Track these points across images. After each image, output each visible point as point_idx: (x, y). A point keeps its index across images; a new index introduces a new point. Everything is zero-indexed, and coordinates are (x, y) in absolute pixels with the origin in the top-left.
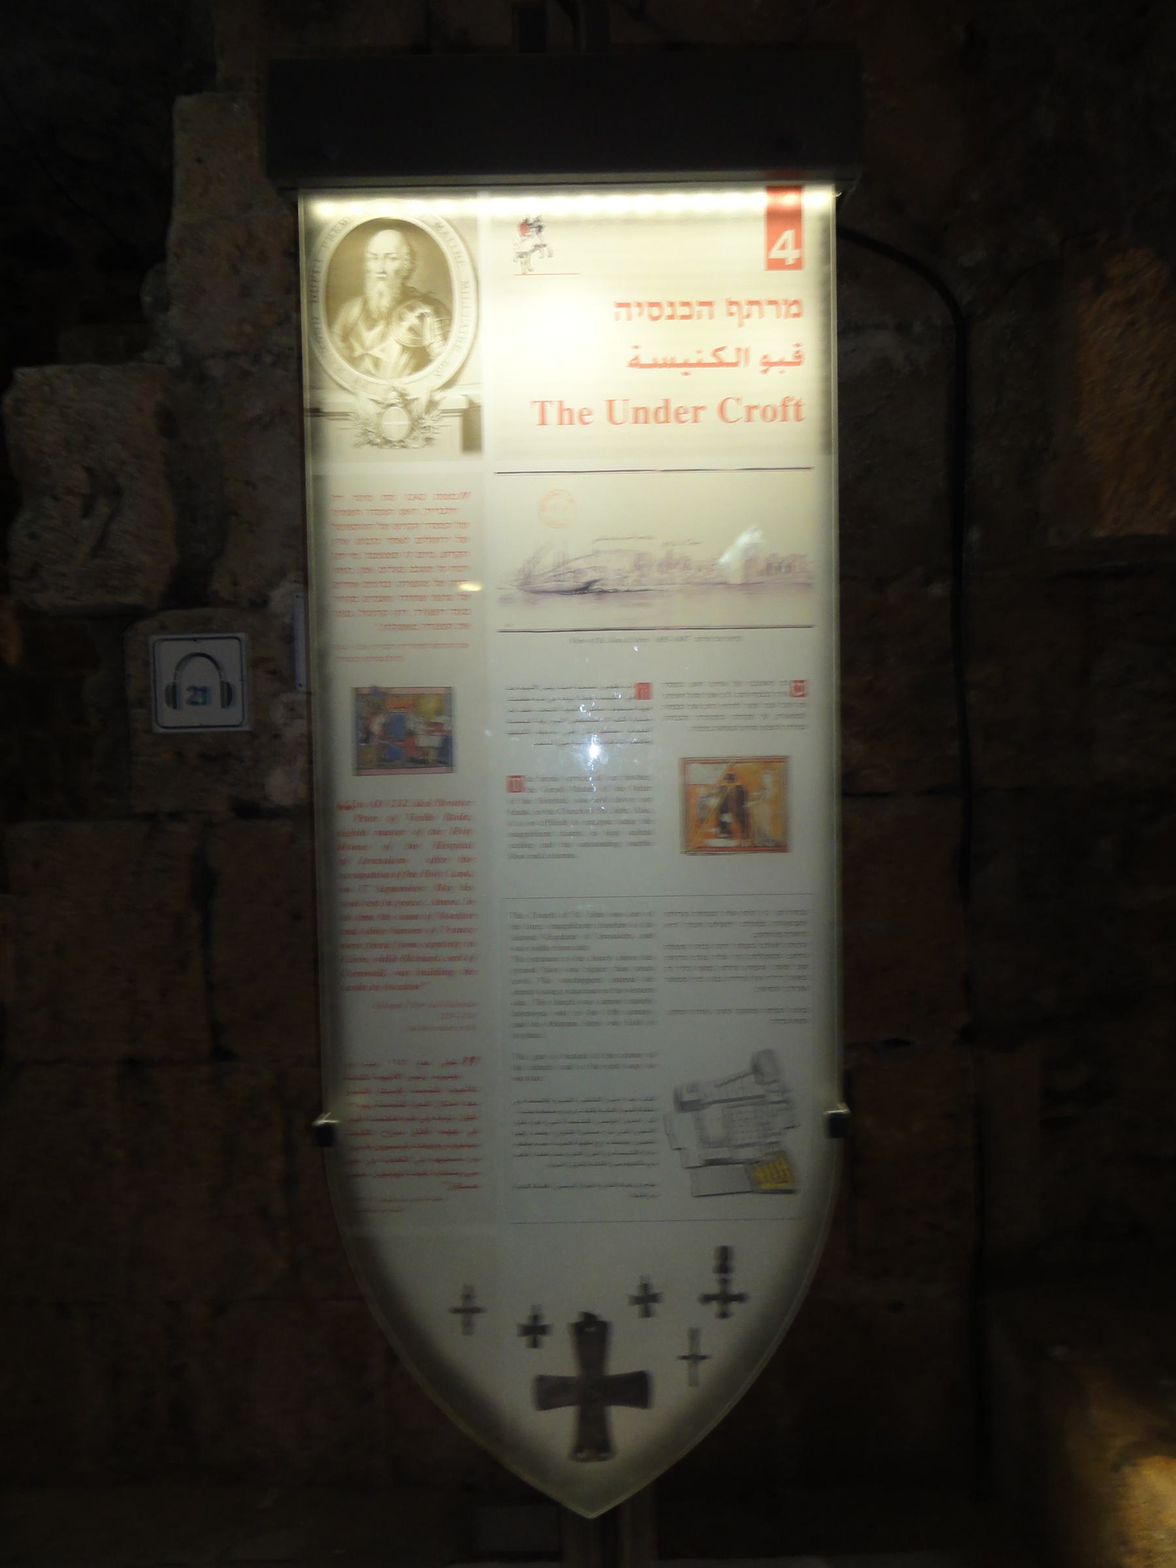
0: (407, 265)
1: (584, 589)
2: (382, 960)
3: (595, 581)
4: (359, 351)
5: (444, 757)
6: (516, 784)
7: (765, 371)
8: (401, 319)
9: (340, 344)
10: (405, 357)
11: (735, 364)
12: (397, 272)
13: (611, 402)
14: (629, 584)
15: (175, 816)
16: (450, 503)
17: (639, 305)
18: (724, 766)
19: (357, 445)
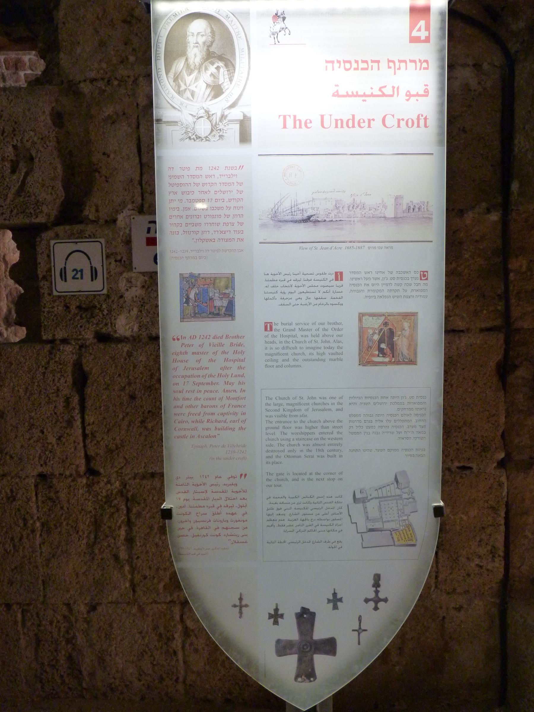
0: (210, 39)
1: (307, 220)
2: (197, 421)
3: (312, 216)
4: (183, 87)
5: (229, 312)
6: (268, 327)
7: (408, 100)
8: (206, 69)
9: (172, 83)
10: (209, 90)
11: (392, 96)
12: (204, 43)
13: (322, 117)
14: (332, 216)
15: (64, 341)
16: (234, 172)
17: (339, 62)
18: (383, 318)
19: (182, 140)
